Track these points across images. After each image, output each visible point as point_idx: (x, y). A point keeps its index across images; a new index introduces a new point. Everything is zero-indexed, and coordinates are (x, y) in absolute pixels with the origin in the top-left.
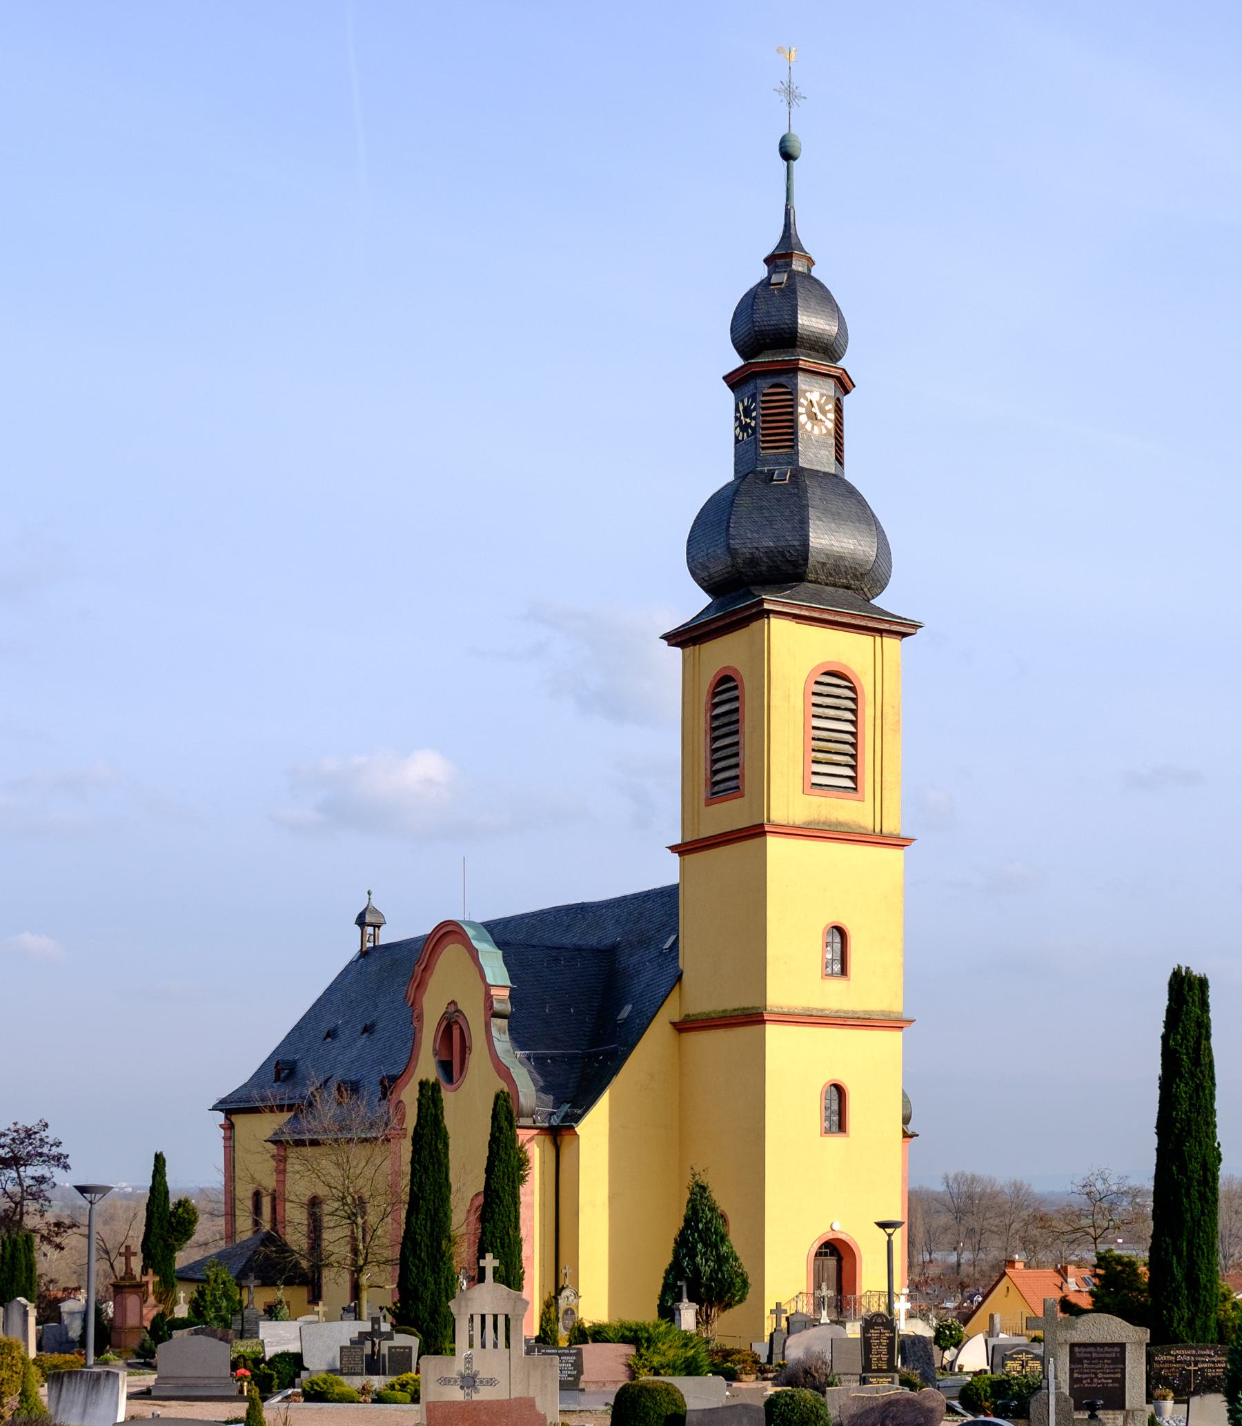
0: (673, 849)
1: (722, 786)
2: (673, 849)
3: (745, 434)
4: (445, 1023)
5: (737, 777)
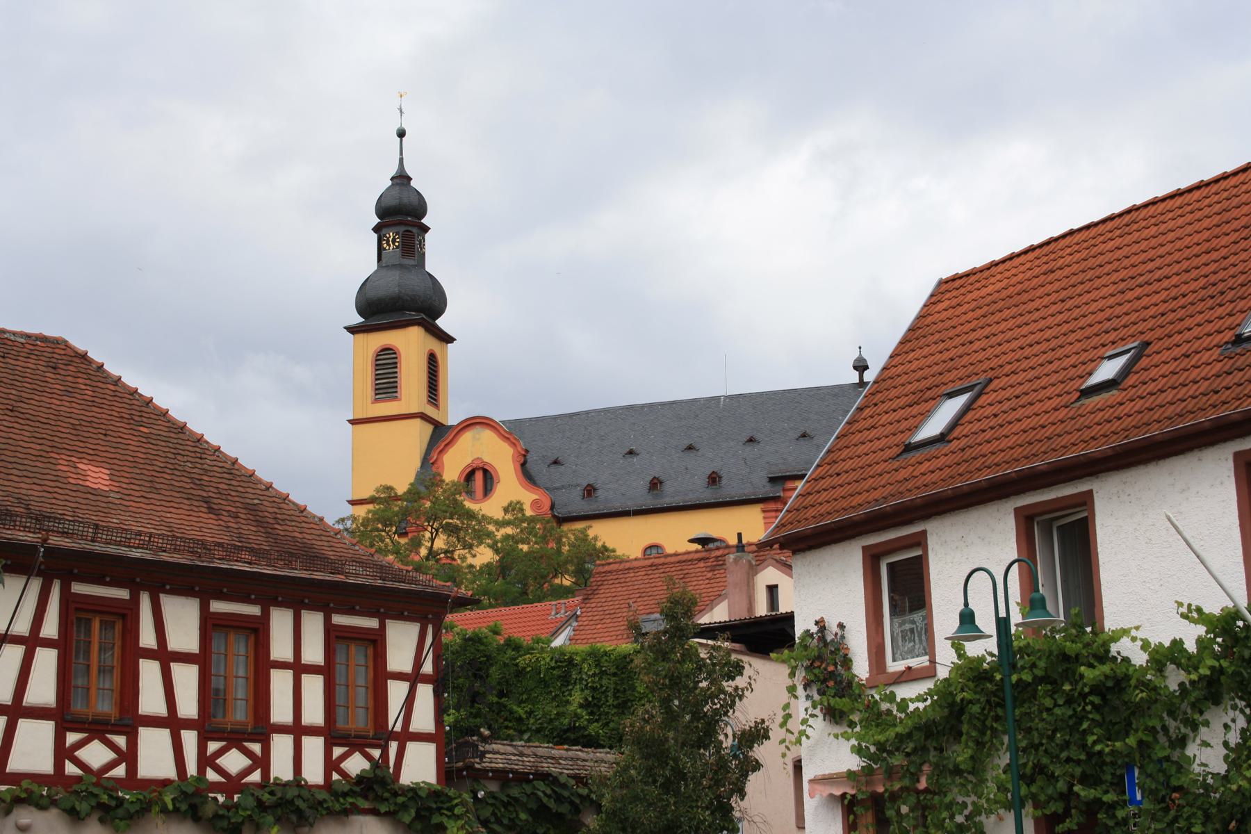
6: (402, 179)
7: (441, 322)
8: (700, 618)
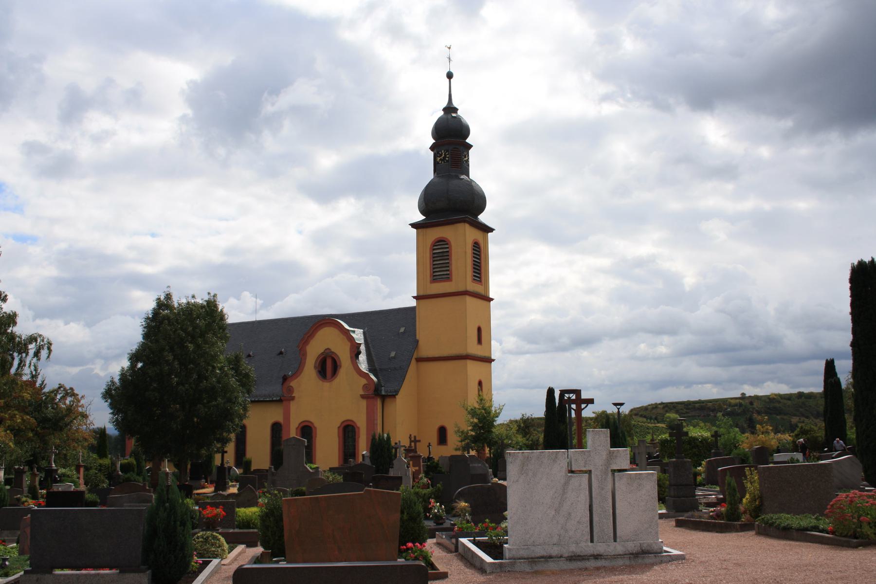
0: (414, 297)
1: (438, 277)
2: (414, 297)
3: (443, 162)
4: (322, 356)
5: (448, 263)
6: (450, 109)
7: (483, 218)
8: (358, 460)
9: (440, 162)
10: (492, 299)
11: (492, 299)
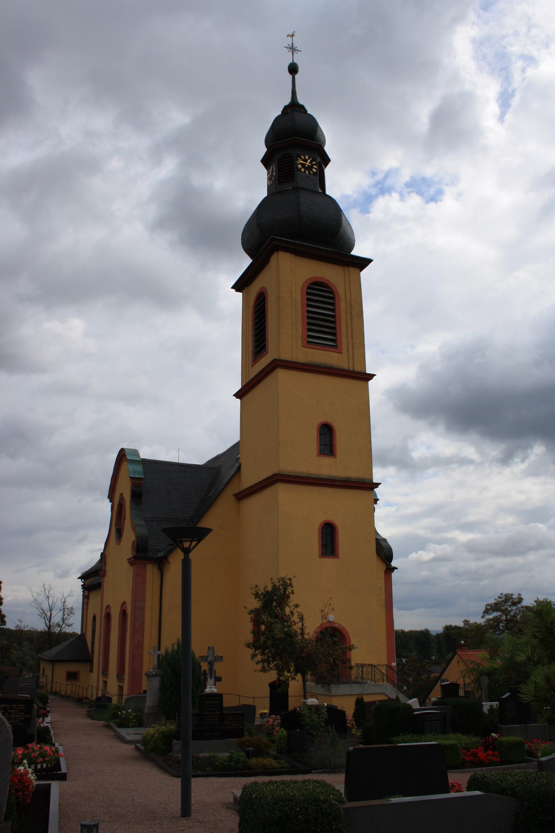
9: (303, 170)
10: (371, 376)
11: (371, 376)
